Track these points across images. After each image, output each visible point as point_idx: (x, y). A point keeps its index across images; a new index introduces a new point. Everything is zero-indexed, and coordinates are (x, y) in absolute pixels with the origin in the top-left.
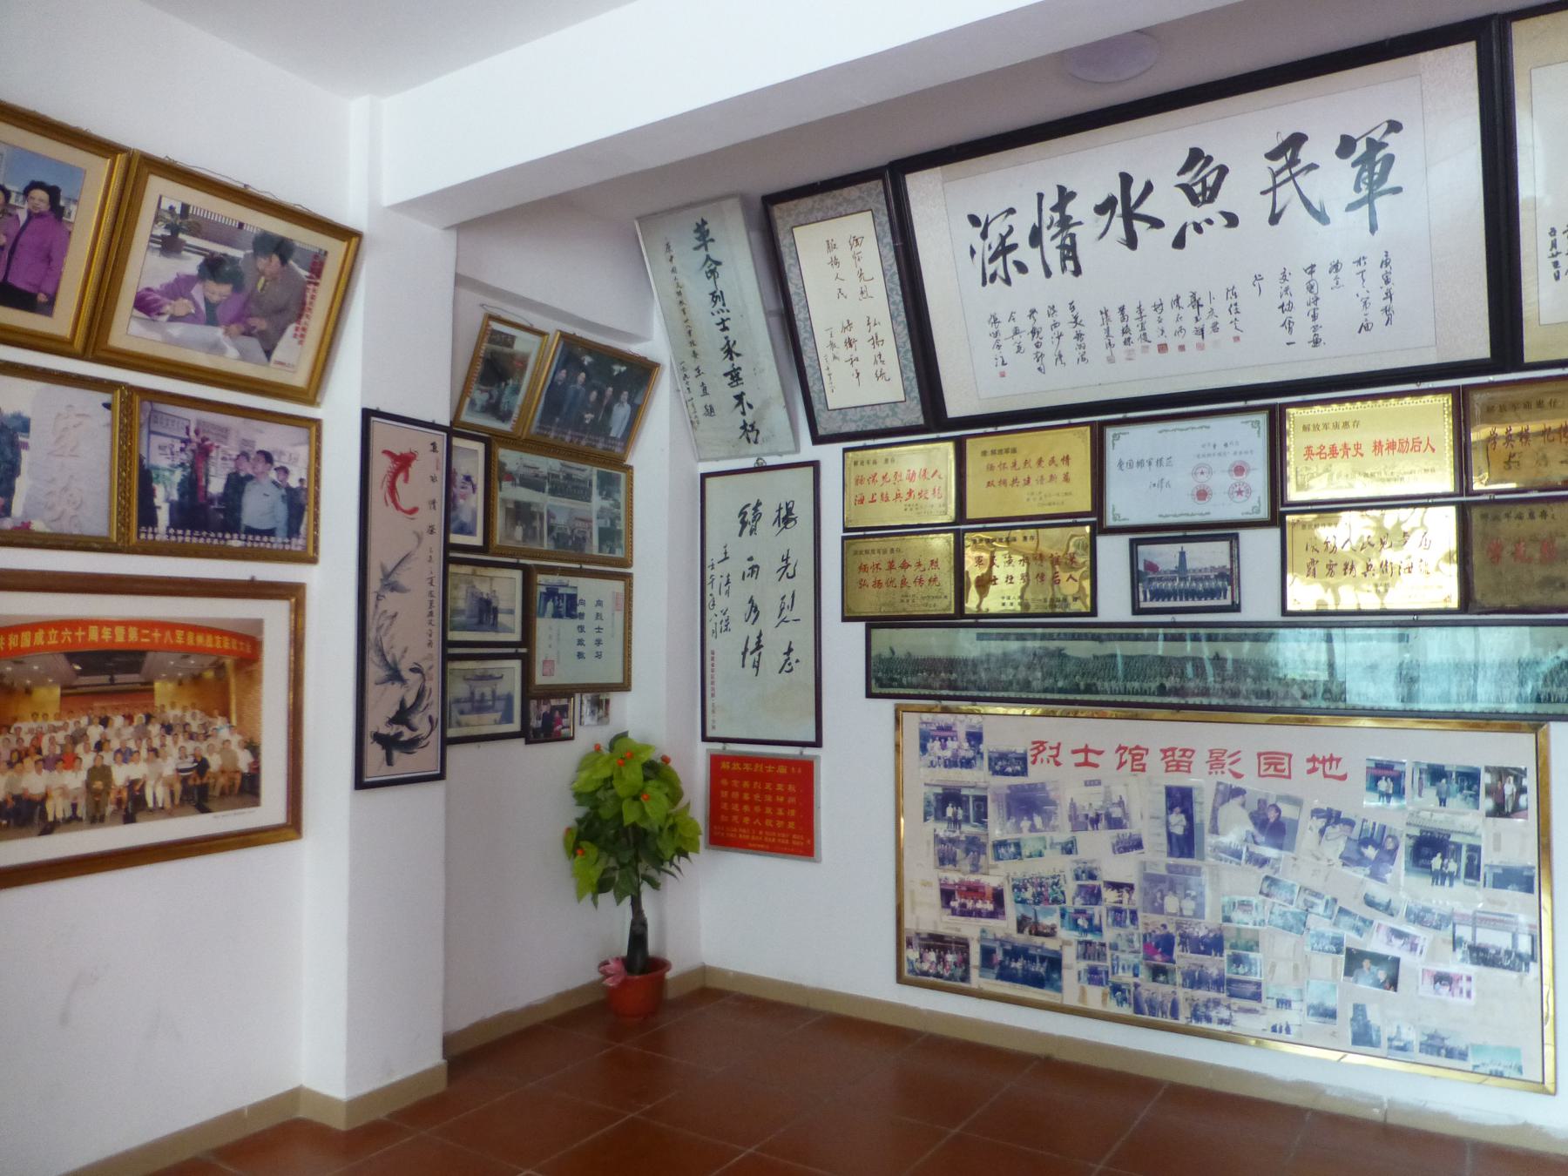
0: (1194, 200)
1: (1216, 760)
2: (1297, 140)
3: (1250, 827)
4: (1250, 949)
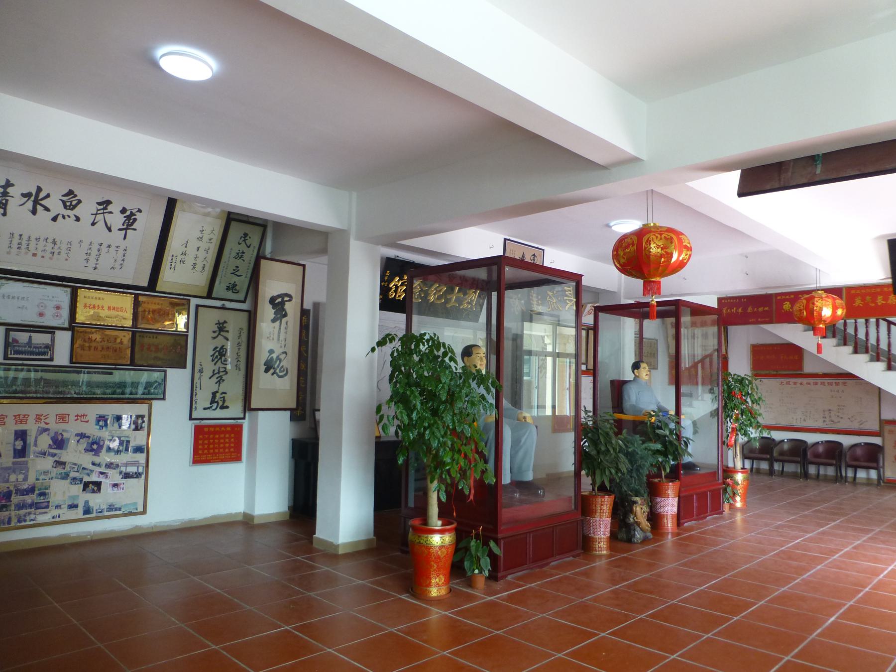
0: (65, 207)
1: (38, 418)
2: (108, 202)
3: (51, 442)
4: (46, 489)
